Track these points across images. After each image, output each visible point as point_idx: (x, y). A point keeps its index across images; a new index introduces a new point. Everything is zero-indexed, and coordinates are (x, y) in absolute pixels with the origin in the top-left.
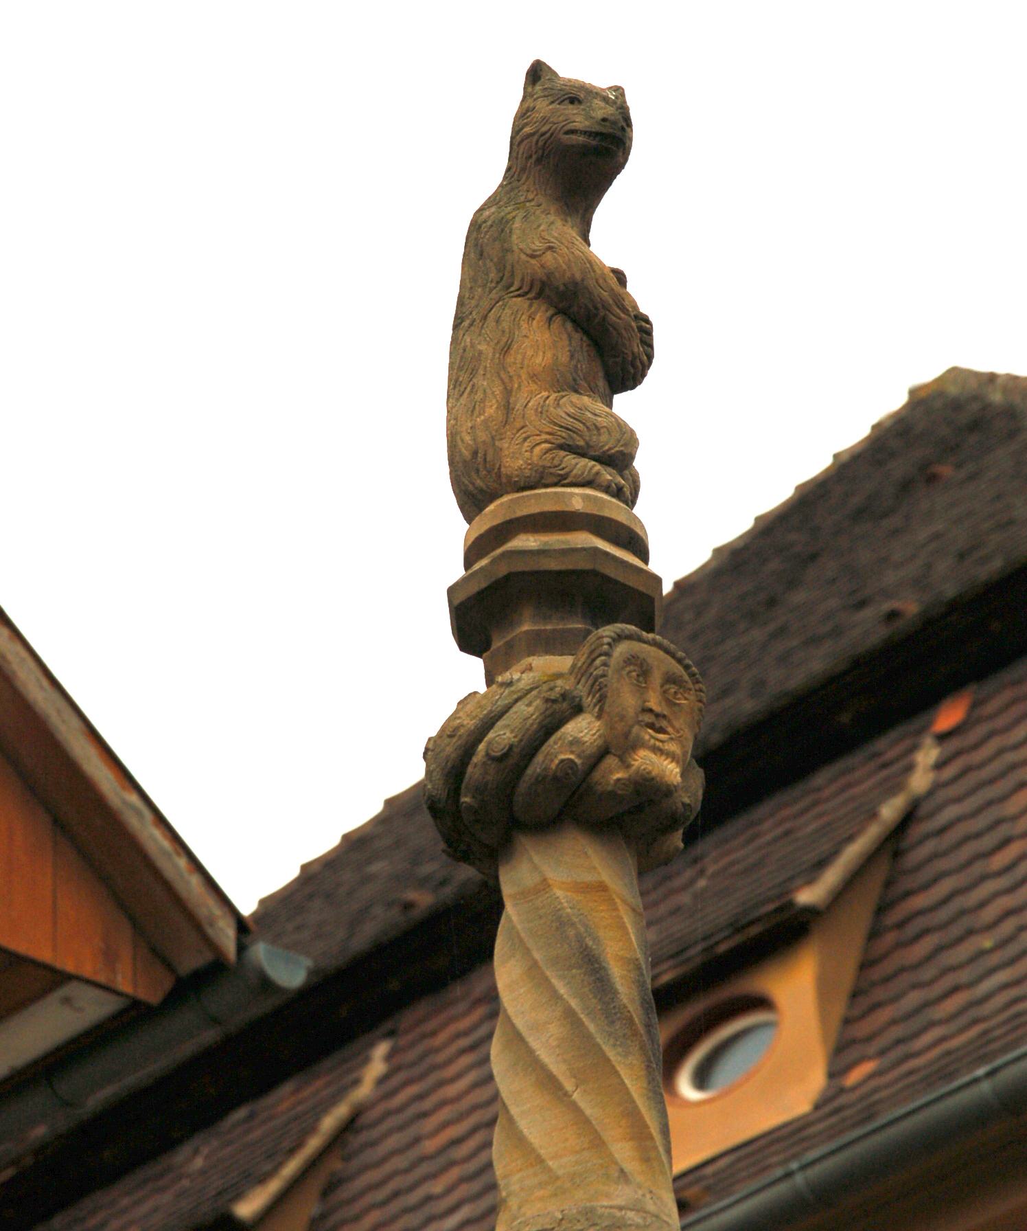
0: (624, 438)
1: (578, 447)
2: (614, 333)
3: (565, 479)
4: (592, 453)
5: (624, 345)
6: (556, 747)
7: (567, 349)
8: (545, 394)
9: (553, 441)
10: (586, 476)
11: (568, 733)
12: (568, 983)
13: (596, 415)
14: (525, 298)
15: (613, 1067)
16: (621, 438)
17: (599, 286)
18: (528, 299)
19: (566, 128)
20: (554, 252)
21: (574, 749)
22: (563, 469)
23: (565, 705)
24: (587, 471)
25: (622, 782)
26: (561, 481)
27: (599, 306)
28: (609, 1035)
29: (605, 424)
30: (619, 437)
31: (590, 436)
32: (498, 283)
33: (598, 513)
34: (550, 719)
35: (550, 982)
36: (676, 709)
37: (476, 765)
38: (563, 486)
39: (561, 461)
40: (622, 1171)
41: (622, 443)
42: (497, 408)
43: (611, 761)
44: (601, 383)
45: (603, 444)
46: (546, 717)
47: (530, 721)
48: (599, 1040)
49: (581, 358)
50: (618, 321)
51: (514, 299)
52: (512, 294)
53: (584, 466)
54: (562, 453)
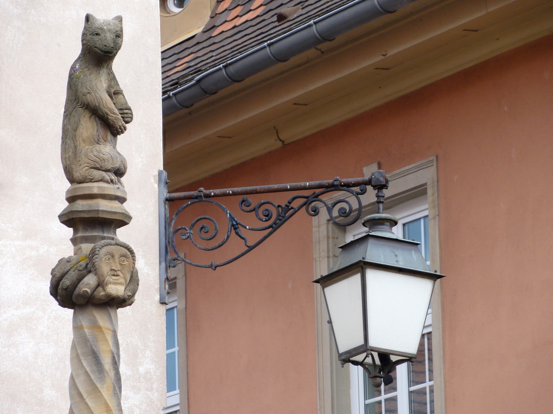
1: (98, 167)
3: (93, 180)
4: (103, 169)
5: (116, 124)
6: (82, 286)
8: (88, 147)
11: (86, 281)
12: (87, 362)
15: (99, 390)
19: (94, 46)
20: (90, 94)
21: (87, 286)
22: (92, 176)
26: (91, 181)
27: (105, 114)
28: (99, 379)
29: (107, 158)
31: (102, 163)
32: (75, 101)
33: (102, 193)
34: (80, 276)
35: (81, 362)
37: (60, 289)
39: (92, 173)
42: (72, 152)
44: (110, 136)
47: (74, 277)
48: (95, 381)
49: (101, 131)
50: (112, 118)
51: (79, 109)
52: (78, 107)
53: (97, 174)
54: (92, 170)
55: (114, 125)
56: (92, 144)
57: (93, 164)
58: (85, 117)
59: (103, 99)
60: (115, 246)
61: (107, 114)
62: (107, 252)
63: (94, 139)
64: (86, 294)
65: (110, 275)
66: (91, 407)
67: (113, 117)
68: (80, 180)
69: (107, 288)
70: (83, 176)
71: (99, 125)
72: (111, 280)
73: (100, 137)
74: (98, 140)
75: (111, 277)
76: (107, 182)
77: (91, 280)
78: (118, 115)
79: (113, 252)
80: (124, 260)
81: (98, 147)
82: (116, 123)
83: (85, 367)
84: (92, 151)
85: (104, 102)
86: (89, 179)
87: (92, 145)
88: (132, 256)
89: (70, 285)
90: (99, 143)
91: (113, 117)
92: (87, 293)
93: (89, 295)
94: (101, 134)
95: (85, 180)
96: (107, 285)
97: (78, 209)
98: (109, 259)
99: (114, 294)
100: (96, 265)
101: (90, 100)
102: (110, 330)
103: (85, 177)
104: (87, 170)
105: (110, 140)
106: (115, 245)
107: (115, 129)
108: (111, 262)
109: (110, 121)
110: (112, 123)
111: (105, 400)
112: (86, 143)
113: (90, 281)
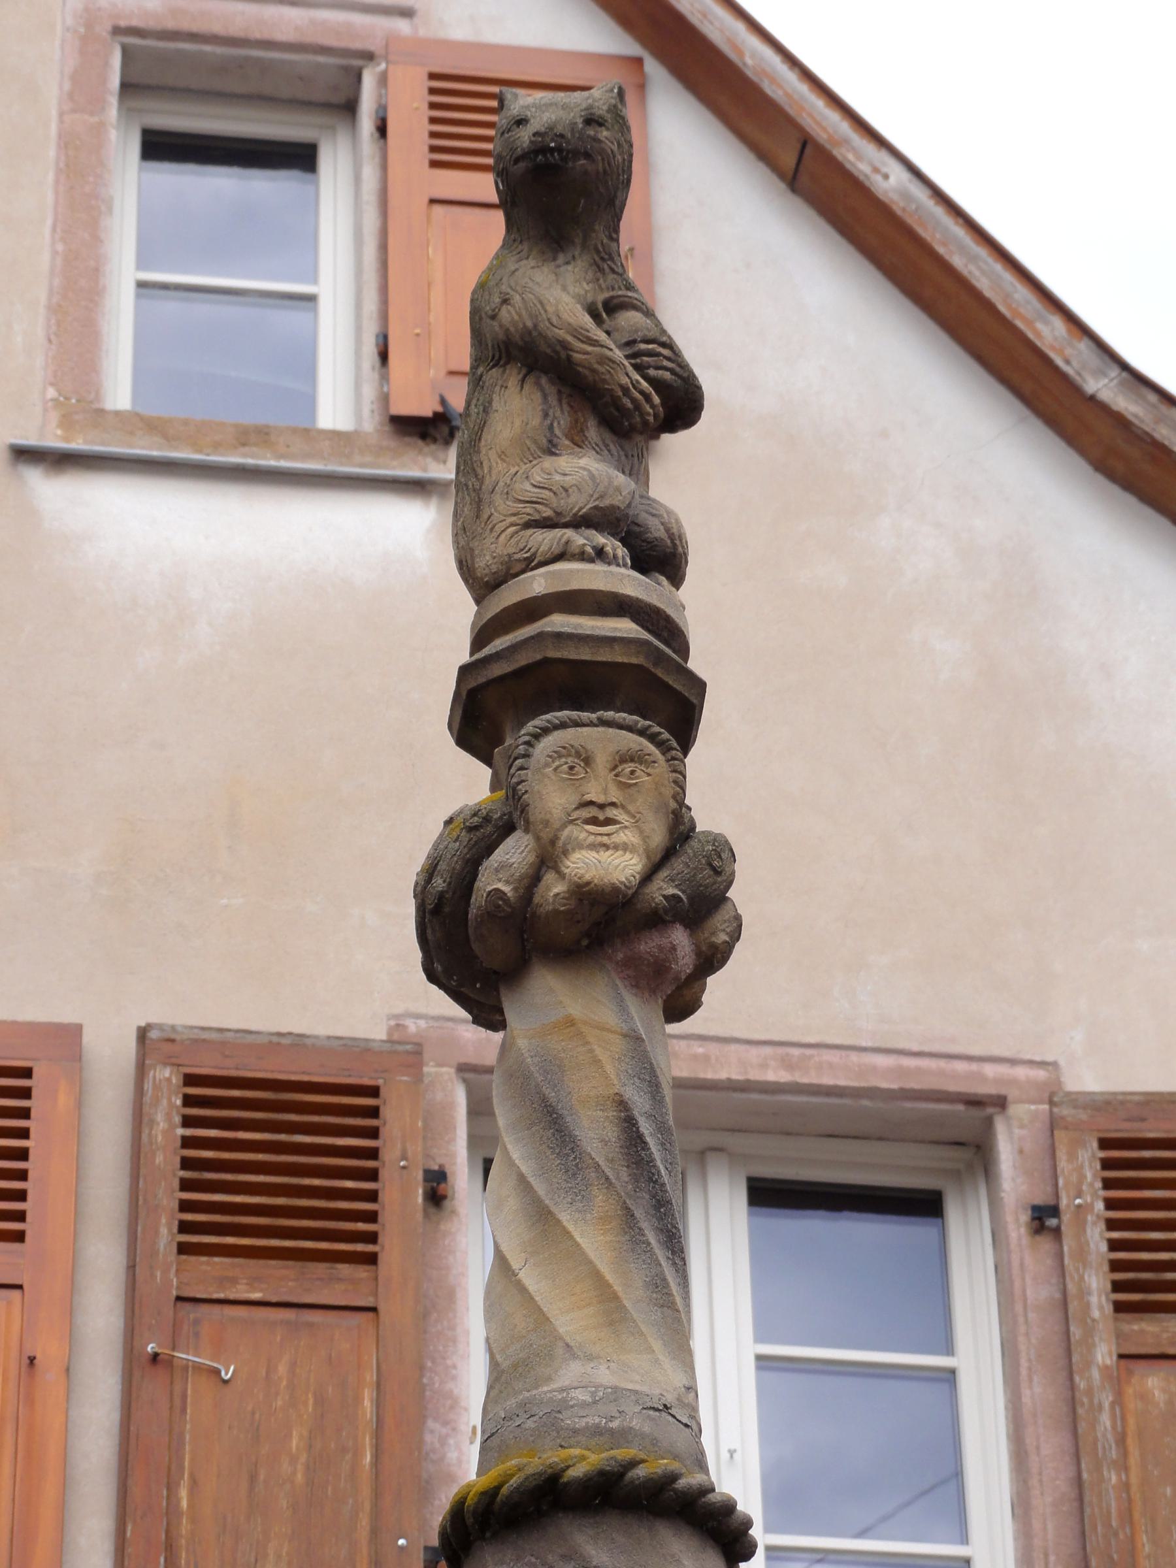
0: (597, 491)
2: (587, 372)
4: (564, 520)
5: (604, 381)
7: (540, 408)
9: (518, 522)
10: (556, 550)
13: (565, 475)
14: (499, 366)
15: (564, 1228)
16: (594, 492)
18: (501, 366)
22: (530, 549)
23: (489, 829)
24: (555, 543)
27: (558, 348)
30: (591, 493)
34: (474, 850)
36: (633, 791)
38: (533, 569)
39: (527, 542)
40: (567, 1345)
41: (596, 496)
43: (549, 877)
45: (571, 506)
46: (470, 849)
49: (558, 413)
56: (531, 459)
57: (531, 512)
58: (506, 387)
59: (545, 302)
61: (565, 345)
62: (564, 748)
63: (535, 442)
66: (533, 1294)
68: (495, 573)
69: (569, 863)
70: (501, 556)
71: (553, 400)
72: (583, 835)
73: (557, 431)
74: (550, 441)
76: (582, 557)
77: (513, 851)
78: (611, 350)
80: (632, 772)
81: (548, 462)
82: (607, 377)
83: (517, 1161)
84: (527, 477)
85: (550, 309)
86: (519, 560)
87: (531, 461)
88: (668, 761)
89: (447, 892)
92: (501, 899)
93: (510, 906)
94: (559, 423)
95: (509, 569)
96: (566, 853)
97: (558, 734)
98: (571, 768)
99: (596, 881)
100: (520, 793)
101: (509, 319)
103: (506, 559)
104: (511, 537)
105: (597, 445)
106: (596, 726)
107: (607, 399)
108: (581, 778)
109: (580, 369)
110: (591, 378)
111: (591, 1262)
112: (507, 459)
113: (507, 857)
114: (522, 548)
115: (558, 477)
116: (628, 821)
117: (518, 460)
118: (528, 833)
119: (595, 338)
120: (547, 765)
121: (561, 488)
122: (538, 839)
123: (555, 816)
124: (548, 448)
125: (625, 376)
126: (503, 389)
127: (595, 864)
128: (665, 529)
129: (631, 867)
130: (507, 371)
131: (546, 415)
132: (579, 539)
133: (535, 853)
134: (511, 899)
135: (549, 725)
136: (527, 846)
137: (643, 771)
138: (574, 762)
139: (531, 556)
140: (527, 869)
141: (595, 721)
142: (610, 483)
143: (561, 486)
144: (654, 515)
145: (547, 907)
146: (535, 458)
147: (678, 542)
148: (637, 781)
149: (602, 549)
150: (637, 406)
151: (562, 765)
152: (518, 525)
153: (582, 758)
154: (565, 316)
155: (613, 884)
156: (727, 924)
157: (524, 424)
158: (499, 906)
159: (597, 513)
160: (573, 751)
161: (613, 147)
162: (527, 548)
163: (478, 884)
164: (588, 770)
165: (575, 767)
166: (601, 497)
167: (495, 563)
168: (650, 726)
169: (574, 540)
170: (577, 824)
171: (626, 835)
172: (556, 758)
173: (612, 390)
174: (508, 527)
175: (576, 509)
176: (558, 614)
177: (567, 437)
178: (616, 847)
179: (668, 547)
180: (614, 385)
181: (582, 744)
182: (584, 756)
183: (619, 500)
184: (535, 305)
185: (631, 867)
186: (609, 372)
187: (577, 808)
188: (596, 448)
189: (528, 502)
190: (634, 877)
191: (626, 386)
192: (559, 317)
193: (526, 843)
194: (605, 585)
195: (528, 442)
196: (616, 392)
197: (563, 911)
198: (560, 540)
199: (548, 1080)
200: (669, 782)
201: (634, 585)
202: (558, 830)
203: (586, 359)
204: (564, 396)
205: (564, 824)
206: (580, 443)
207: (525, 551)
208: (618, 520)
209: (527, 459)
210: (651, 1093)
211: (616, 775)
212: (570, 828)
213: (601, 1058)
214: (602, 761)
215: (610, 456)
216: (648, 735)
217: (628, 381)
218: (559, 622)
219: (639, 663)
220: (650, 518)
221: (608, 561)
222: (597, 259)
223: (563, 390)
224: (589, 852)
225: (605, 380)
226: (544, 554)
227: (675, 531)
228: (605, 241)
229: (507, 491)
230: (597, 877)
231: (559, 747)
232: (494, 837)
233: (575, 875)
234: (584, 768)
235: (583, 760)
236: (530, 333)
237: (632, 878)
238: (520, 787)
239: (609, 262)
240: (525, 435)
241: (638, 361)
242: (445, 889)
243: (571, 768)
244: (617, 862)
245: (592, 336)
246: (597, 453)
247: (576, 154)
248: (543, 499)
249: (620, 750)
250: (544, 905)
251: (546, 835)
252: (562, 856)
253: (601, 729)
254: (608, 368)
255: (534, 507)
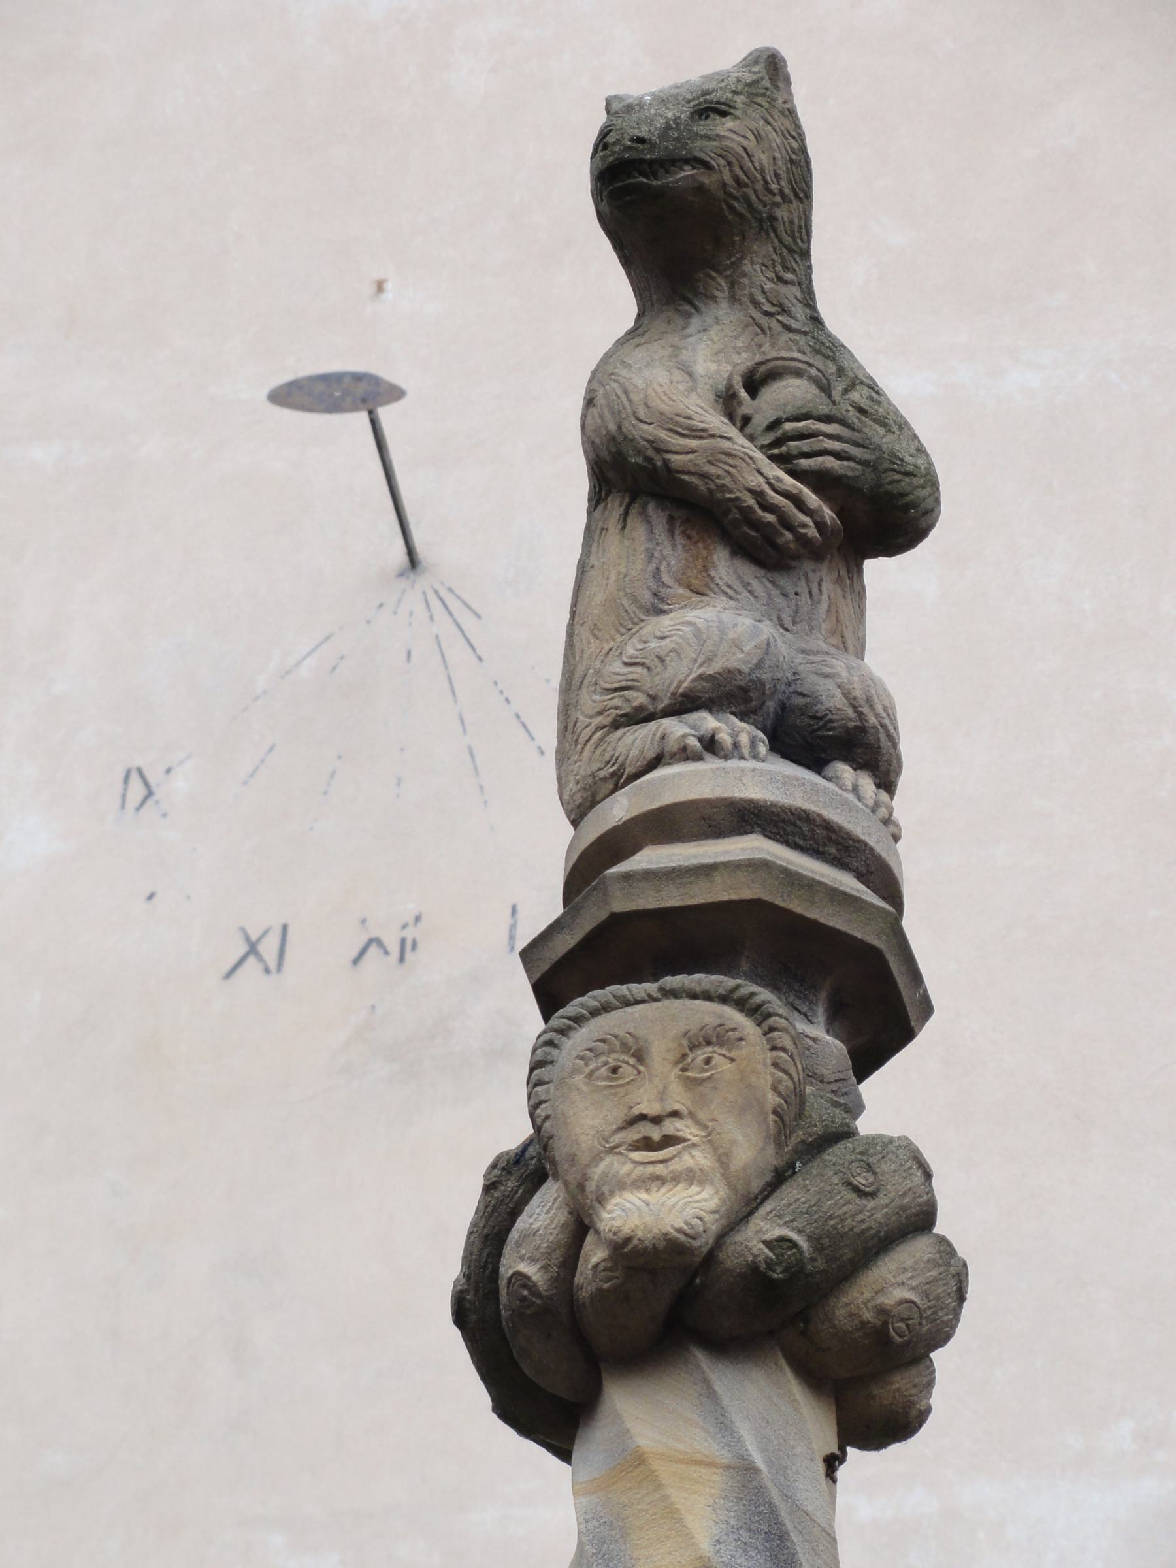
1: (640, 708)
2: (694, 479)
4: (661, 706)
10: (650, 754)
17: (641, 421)
22: (617, 759)
24: (648, 743)
25: (601, 1267)
27: (650, 453)
30: (694, 656)
38: (622, 787)
41: (700, 661)
49: (668, 551)
50: (690, 456)
55: (719, 495)
56: (631, 626)
57: (620, 704)
59: (630, 388)
60: (655, 1004)
62: (603, 1041)
63: (634, 599)
64: (525, 1293)
65: (622, 1149)
67: (693, 452)
73: (666, 578)
75: (627, 1156)
76: (685, 754)
79: (641, 1033)
80: (708, 1061)
82: (727, 481)
85: (636, 398)
86: (604, 779)
87: (629, 630)
89: (467, 1291)
90: (666, 607)
91: (693, 452)
92: (525, 1286)
93: (539, 1295)
94: (669, 565)
96: (601, 1200)
99: (640, 1234)
102: (710, 1465)
103: (590, 780)
105: (730, 587)
106: (656, 1000)
108: (628, 1083)
109: (686, 477)
113: (531, 1221)
114: (608, 759)
115: (654, 644)
116: (697, 1136)
117: (613, 632)
118: (557, 1180)
119: (702, 425)
120: (575, 1071)
121: (656, 659)
122: (566, 1184)
123: (584, 1145)
124: (653, 604)
125: (757, 474)
126: (604, 532)
127: (639, 1209)
128: (843, 694)
129: (696, 1205)
130: (609, 505)
131: (651, 557)
132: (676, 729)
133: (568, 1209)
134: (539, 1284)
135: (584, 1011)
136: (555, 1199)
137: (724, 1056)
138: (618, 1060)
139: (619, 769)
140: (557, 1235)
141: (656, 994)
142: (722, 632)
143: (657, 656)
144: (827, 676)
145: (589, 1288)
146: (636, 624)
147: (865, 710)
148: (713, 1072)
149: (713, 736)
150: (786, 523)
151: (597, 1069)
152: (604, 727)
153: (631, 1052)
154: (656, 403)
155: (666, 1234)
156: (909, 1274)
157: (622, 576)
158: (524, 1299)
159: (705, 684)
160: (618, 1044)
161: (745, 143)
162: (614, 758)
163: (502, 1270)
164: (642, 1068)
165: (619, 1067)
166: (709, 660)
167: (579, 791)
168: (737, 987)
169: (672, 732)
170: (620, 1153)
171: (693, 1157)
172: (590, 1059)
173: (737, 499)
174: (594, 733)
175: (675, 685)
176: (650, 847)
177: (679, 582)
178: (676, 1179)
179: (850, 720)
180: (740, 492)
181: (632, 1030)
182: (634, 1048)
183: (739, 660)
184: (619, 397)
185: (696, 1205)
186: (728, 472)
187: (621, 1129)
188: (728, 591)
189: (616, 690)
190: (701, 1219)
191: (758, 489)
192: (648, 407)
193: (556, 1195)
194: (713, 790)
195: (626, 603)
196: (745, 501)
197: (608, 1290)
198: (654, 735)
199: (601, 1553)
200: (765, 1065)
201: (761, 781)
202: (587, 1166)
203: (690, 461)
204: (678, 523)
205: (598, 1155)
206: (701, 589)
207: (611, 763)
208: (745, 690)
209: (624, 627)
210: (771, 1549)
211: (684, 1070)
212: (608, 1159)
213: (679, 1507)
214: (660, 1052)
215: (752, 598)
216: (734, 1000)
217: (761, 480)
218: (650, 858)
219: (755, 897)
220: (822, 681)
221: (723, 753)
222: (757, 315)
223: (676, 515)
224: (635, 1191)
225: (723, 485)
226: (634, 763)
227: (858, 693)
228: (769, 286)
229: (596, 681)
230: (642, 1227)
231: (598, 1041)
232: (518, 1195)
233: (610, 1231)
234: (634, 1066)
235: (633, 1055)
236: (614, 439)
237: (698, 1221)
238: (539, 1111)
239: (780, 318)
240: (622, 593)
241: (784, 449)
242: (465, 1287)
243: (615, 1070)
244: (673, 1200)
245: (699, 424)
246: (731, 598)
247: (672, 162)
248: (634, 680)
249: (689, 1031)
250: (585, 1285)
251: (572, 1176)
252: (597, 1205)
253: (666, 1002)
254: (727, 468)
255: (622, 696)
